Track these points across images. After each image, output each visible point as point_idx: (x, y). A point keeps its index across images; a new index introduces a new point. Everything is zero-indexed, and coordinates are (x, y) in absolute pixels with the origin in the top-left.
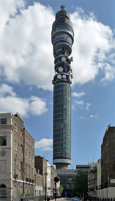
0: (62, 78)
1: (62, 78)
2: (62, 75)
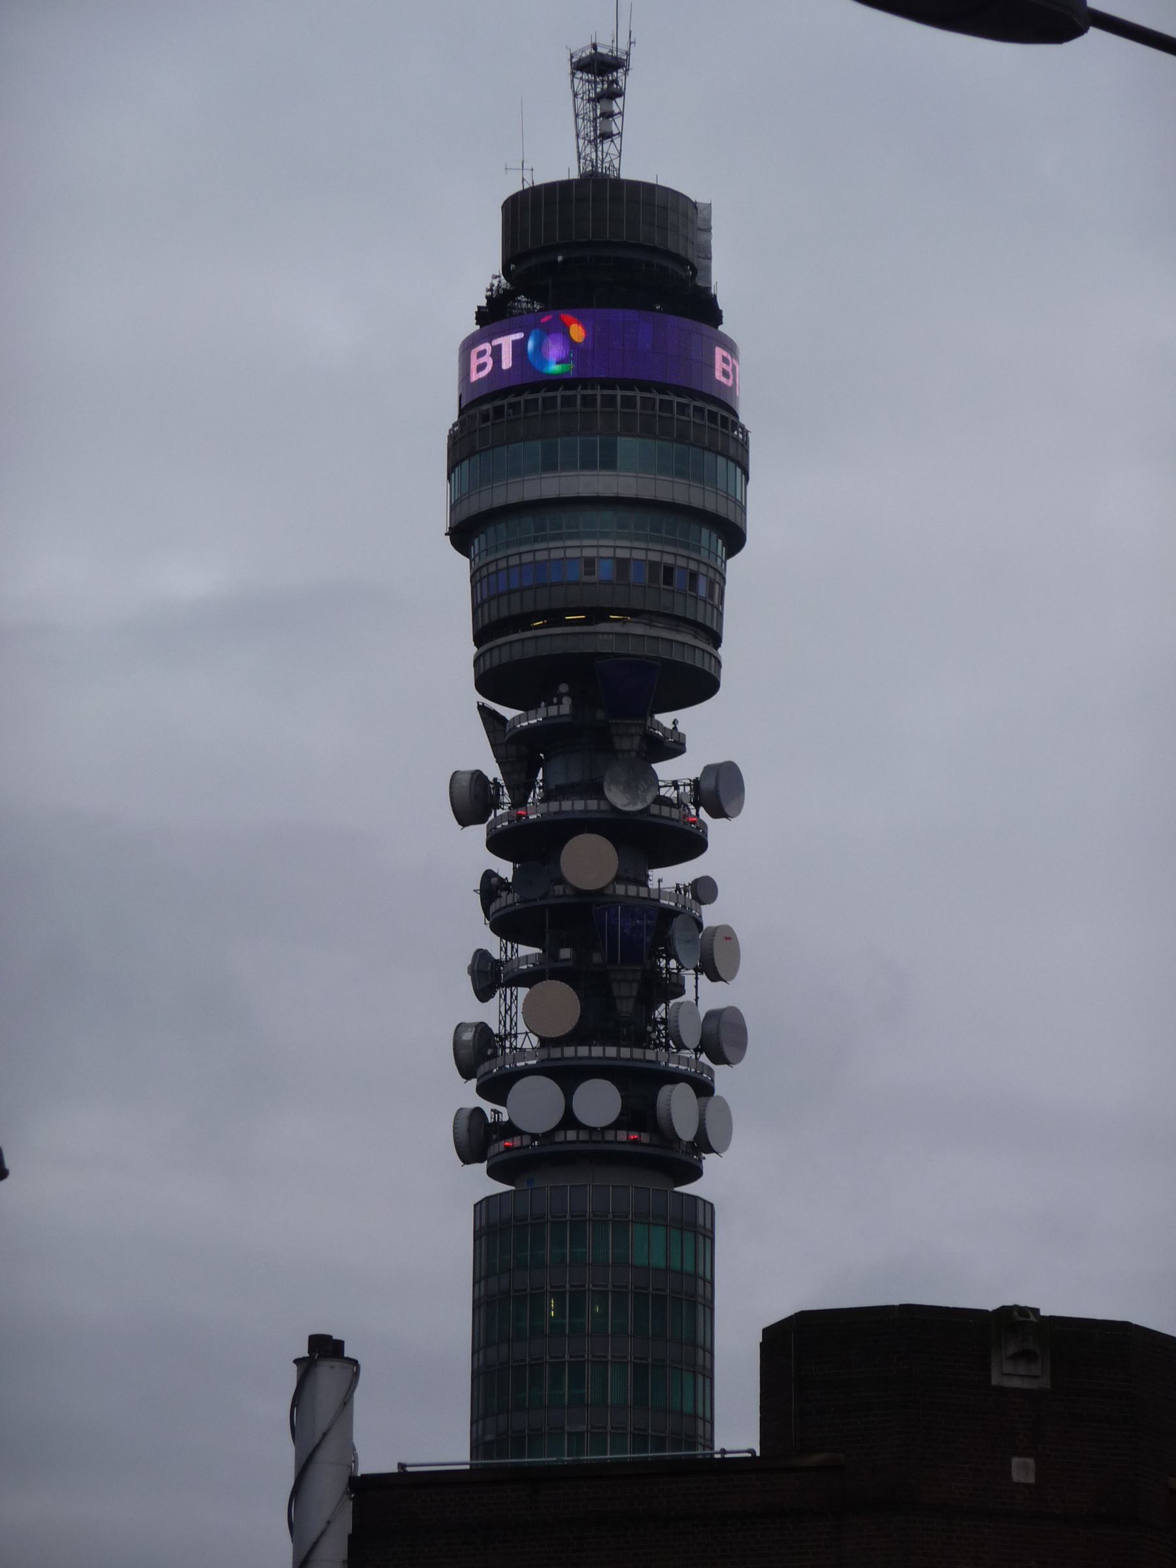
0: (569, 1120)
1: (569, 1120)
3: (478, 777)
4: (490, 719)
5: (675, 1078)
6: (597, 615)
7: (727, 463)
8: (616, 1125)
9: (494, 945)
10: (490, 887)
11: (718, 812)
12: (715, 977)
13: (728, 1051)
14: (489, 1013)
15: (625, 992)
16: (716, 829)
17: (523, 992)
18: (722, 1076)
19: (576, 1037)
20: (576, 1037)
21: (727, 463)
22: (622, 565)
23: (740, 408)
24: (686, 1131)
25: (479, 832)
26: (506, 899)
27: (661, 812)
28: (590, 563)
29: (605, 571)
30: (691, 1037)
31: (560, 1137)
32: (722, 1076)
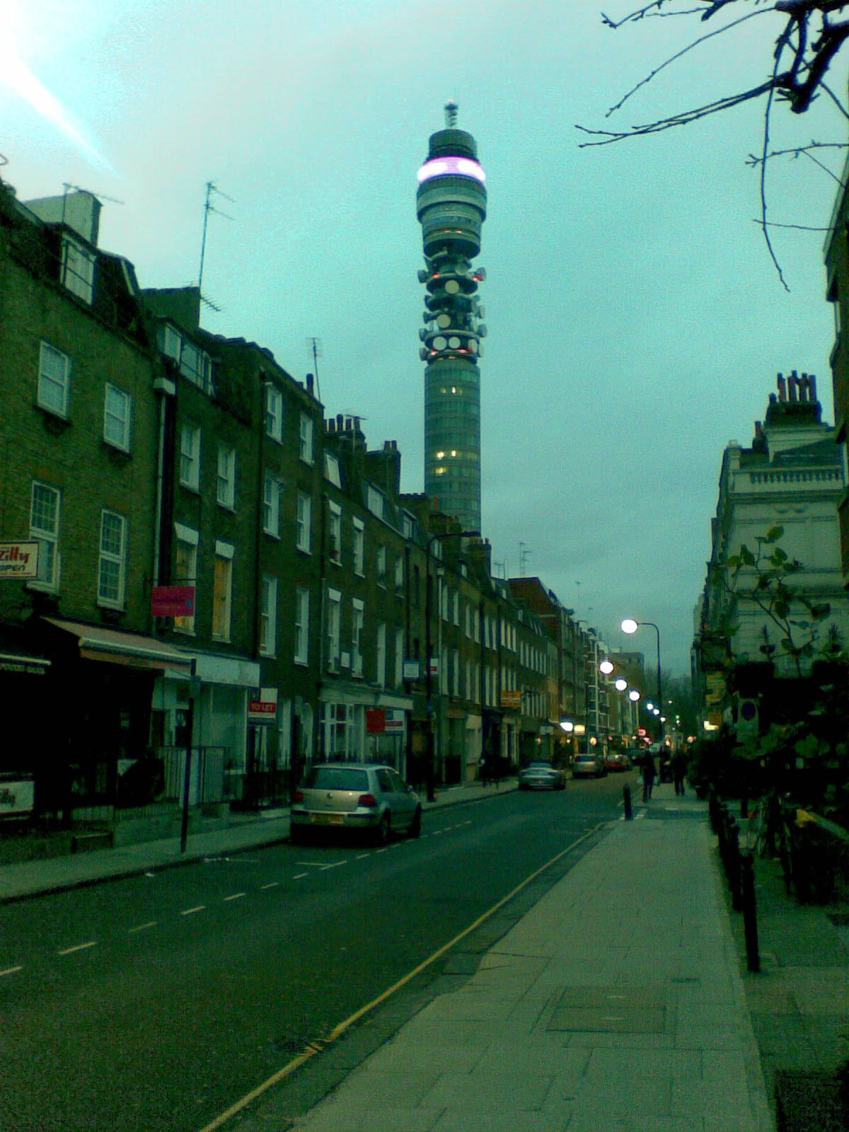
0: (448, 347)
1: (448, 347)
2: (447, 337)
3: (424, 271)
4: (426, 260)
5: (472, 338)
6: (454, 229)
7: (806, 153)
8: (459, 348)
9: (428, 311)
10: (427, 298)
11: (481, 280)
12: (480, 317)
13: (484, 334)
14: (427, 327)
15: (460, 318)
16: (480, 284)
17: (435, 321)
18: (482, 340)
19: (449, 328)
20: (449, 328)
21: (806, 153)
22: (459, 218)
23: (435, 164)
24: (475, 350)
25: (425, 285)
26: (429, 300)
27: (163, 707)
28: (452, 217)
29: (456, 219)
30: (476, 328)
31: (445, 351)
32: (482, 340)
